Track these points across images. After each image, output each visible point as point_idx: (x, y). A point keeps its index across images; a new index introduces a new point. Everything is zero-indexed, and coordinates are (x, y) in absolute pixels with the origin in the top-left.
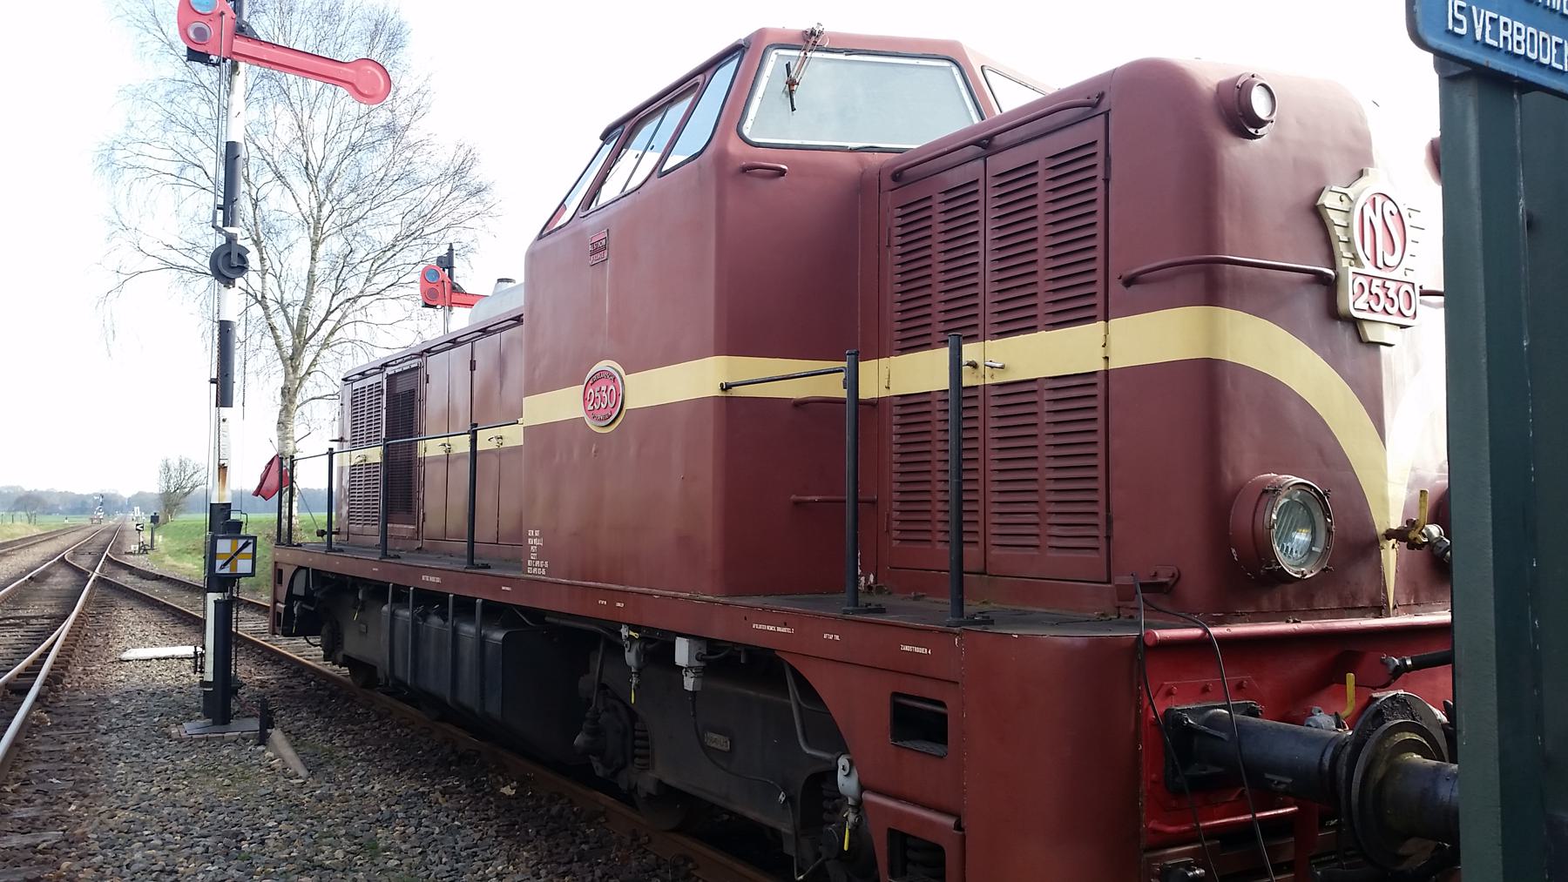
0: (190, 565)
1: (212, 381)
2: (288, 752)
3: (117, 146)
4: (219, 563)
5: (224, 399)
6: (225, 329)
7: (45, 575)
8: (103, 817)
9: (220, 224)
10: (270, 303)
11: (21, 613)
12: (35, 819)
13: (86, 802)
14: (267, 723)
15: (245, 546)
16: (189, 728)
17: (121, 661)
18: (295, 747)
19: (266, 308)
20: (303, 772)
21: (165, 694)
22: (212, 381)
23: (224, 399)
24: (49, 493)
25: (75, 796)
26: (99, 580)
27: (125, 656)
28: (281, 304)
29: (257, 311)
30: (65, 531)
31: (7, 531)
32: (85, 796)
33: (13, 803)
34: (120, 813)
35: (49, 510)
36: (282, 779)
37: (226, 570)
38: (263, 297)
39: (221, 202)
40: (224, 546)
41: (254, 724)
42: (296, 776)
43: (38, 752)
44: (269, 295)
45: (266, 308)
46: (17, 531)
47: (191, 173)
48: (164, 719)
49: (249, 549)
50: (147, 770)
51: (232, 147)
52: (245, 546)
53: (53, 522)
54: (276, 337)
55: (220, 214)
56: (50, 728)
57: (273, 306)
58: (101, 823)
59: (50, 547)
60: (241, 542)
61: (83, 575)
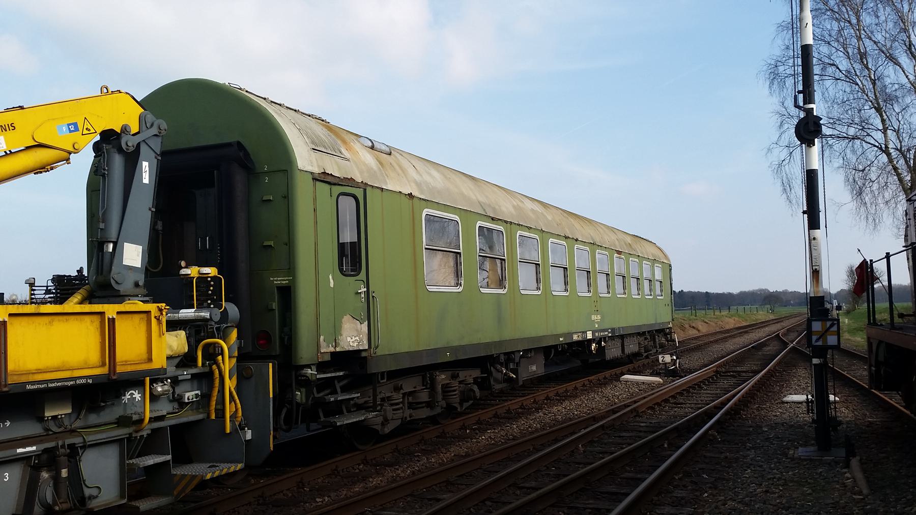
0: (859, 339)
1: (804, 212)
2: (859, 475)
3: (779, 64)
4: (814, 338)
5: (814, 223)
6: (811, 178)
7: (764, 344)
8: (719, 503)
9: (801, 104)
10: (892, 151)
11: (739, 369)
12: (682, 498)
13: (715, 492)
14: (851, 453)
15: (832, 326)
16: (801, 452)
17: (783, 403)
18: (864, 471)
19: (889, 155)
20: (865, 491)
21: (800, 427)
22: (804, 212)
23: (814, 223)
24: (785, 293)
25: (710, 488)
26: (793, 348)
27: (785, 399)
28: (900, 151)
29: (884, 158)
30: (795, 316)
31: (754, 317)
32: (716, 488)
33: (676, 487)
34: (730, 503)
35: (786, 304)
36: (849, 494)
37: (820, 343)
38: (887, 147)
39: (801, 88)
40: (817, 326)
41: (842, 453)
42: (860, 493)
43: (705, 457)
44: (891, 145)
45: (889, 155)
46: (760, 317)
47: (831, 70)
48: (790, 444)
49: (835, 328)
50: (762, 476)
51: (806, 51)
52: (832, 326)
53: (784, 311)
54: (898, 175)
55: (801, 96)
56: (719, 443)
57: (894, 153)
58: (716, 507)
59: (774, 328)
60: (829, 324)
61: (785, 345)
